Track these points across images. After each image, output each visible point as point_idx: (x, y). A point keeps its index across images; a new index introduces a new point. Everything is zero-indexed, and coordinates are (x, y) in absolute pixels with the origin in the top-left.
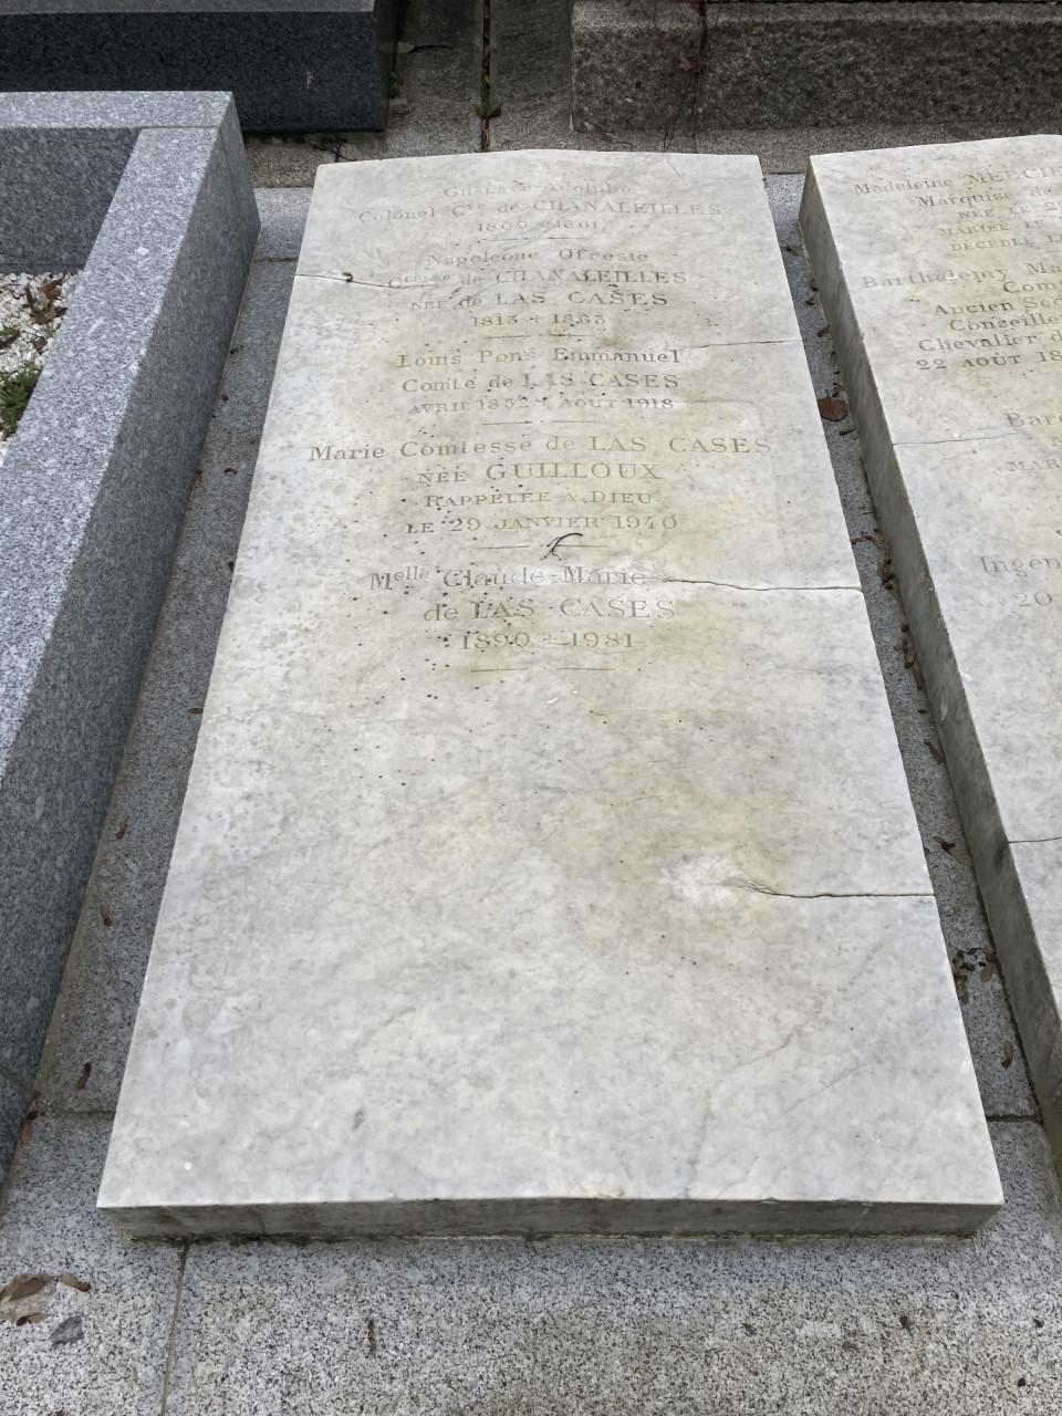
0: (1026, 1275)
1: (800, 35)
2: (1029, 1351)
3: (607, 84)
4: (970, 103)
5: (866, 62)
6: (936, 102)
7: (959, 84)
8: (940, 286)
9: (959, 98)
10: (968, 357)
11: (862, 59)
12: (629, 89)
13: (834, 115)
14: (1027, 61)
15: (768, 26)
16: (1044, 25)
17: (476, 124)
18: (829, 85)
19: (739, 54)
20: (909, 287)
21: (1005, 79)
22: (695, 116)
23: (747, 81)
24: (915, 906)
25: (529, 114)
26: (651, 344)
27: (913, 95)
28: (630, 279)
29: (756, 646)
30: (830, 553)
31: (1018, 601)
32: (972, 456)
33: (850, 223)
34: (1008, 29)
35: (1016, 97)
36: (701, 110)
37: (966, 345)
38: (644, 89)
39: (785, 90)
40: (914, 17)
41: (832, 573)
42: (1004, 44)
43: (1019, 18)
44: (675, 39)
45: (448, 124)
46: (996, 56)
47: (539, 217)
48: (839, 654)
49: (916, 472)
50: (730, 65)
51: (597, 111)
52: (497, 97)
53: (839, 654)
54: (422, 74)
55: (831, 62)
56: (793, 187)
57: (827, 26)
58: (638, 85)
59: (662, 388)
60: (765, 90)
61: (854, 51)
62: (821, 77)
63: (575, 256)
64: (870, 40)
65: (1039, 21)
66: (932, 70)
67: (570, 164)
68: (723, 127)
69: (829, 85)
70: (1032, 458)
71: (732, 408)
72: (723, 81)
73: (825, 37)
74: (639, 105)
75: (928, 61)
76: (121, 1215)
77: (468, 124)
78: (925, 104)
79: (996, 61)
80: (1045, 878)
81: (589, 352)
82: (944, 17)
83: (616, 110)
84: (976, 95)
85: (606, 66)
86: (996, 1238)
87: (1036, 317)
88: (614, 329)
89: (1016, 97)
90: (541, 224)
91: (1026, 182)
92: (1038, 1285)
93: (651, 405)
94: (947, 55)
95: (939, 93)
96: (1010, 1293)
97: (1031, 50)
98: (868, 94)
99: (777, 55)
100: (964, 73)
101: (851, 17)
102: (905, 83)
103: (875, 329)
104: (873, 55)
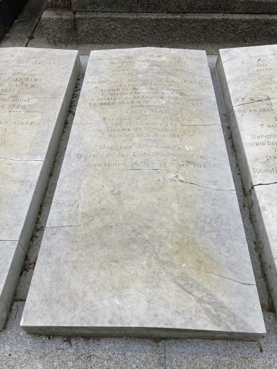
0: (12, 342)
1: (99, 21)
2: (5, 362)
3: (53, 31)
4: (147, 39)
5: (118, 28)
6: (138, 38)
7: (142, 34)
8: (105, 84)
9: (144, 37)
10: (102, 103)
11: (116, 27)
12: (59, 33)
13: (112, 41)
14: (159, 28)
15: (90, 18)
16: (161, 19)
17: (27, 40)
18: (110, 33)
19: (85, 25)
20: (97, 84)
21: (154, 33)
22: (77, 40)
23: (89, 32)
24: (11, 244)
25: (40, 38)
26: (24, 97)
27: (131, 36)
28: (28, 80)
29: (8, 175)
30: (41, 152)
31: (81, 165)
32: (90, 128)
33: (91, 68)
34: (152, 20)
35: (158, 38)
36: (78, 39)
37: (104, 99)
38: (63, 33)
39: (99, 34)
40: (127, 16)
41: (38, 157)
42: (152, 24)
43: (154, 17)
44: (67, 20)
45: (19, 40)
46: (150, 27)
47: (13, 64)
48: (28, 178)
49: (74, 131)
50: (83, 28)
51: (52, 38)
52: (35, 35)
53: (28, 178)
54: (17, 28)
55: (109, 28)
56: (214, 59)
57: (105, 18)
58: (61, 32)
59: (21, 108)
60: (94, 34)
61: (114, 25)
62: (107, 31)
63: (16, 74)
64: (117, 22)
65: (160, 18)
66: (135, 30)
67: (28, 51)
68: (86, 43)
69: (110, 33)
70: (104, 129)
71: (36, 114)
72: (82, 32)
73: (106, 21)
74: (63, 37)
75: (133, 28)
76: (25, 328)
77: (24, 41)
78: (135, 38)
79: (151, 28)
80: (49, 237)
81: (6, 99)
82: (135, 17)
83: (57, 38)
84: (148, 37)
85: (51, 27)
86: (9, 332)
87: (124, 93)
88: (16, 93)
89: (158, 38)
90: (12, 66)
91: (139, 59)
92: (14, 345)
93: (15, 112)
94: (137, 26)
95: (138, 36)
96: (6, 347)
97: (159, 25)
98: (120, 36)
99: (95, 26)
100: (143, 31)
101: (111, 16)
102: (129, 33)
103: (83, 95)
104: (119, 26)
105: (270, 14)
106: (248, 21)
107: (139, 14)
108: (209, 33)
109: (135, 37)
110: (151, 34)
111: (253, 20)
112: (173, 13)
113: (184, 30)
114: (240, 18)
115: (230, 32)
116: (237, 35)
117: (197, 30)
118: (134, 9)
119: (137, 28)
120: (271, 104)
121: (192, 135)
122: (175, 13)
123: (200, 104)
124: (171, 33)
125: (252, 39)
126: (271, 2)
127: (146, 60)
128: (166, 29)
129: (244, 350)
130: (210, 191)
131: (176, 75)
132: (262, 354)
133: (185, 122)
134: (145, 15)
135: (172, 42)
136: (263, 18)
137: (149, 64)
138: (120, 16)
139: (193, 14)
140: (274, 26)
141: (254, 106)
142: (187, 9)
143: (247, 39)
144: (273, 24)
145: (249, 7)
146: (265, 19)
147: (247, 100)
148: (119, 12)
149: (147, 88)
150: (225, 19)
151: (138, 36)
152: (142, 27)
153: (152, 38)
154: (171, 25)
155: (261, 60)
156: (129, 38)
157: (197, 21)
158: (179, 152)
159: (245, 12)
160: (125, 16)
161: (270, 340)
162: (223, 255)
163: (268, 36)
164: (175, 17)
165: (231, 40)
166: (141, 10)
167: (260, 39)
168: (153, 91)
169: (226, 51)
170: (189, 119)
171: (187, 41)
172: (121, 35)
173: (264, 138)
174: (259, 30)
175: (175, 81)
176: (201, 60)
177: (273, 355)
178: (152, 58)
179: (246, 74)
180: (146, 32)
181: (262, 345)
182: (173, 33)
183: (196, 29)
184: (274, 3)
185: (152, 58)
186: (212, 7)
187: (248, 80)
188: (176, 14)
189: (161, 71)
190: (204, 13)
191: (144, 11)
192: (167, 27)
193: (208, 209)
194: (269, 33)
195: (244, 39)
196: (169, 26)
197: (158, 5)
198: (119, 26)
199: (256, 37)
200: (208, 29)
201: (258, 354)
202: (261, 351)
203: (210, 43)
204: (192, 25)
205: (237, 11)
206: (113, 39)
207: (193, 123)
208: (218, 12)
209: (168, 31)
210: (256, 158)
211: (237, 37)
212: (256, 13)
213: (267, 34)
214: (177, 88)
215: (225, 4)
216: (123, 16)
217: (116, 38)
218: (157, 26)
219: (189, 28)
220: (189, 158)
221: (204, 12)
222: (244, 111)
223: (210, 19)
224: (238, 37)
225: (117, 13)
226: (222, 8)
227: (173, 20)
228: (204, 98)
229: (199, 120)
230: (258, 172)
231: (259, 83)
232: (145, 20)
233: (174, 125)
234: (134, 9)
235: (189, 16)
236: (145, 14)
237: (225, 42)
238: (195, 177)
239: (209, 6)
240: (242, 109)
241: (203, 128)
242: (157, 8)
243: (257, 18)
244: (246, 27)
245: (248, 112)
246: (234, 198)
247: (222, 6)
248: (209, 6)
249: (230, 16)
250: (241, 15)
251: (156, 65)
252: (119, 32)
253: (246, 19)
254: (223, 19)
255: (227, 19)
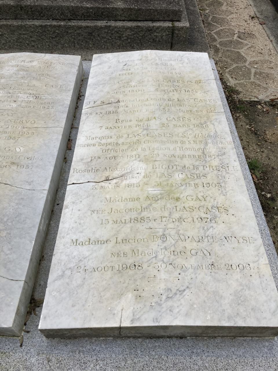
7: (31, 40)
9: (33, 44)
11: (4, 33)
13: (3, 47)
14: (46, 34)
40: (12, 23)
42: (37, 30)
65: (44, 24)
66: (23, 36)
75: (20, 34)
76: (41, 331)
78: (25, 44)
79: (38, 34)
82: (20, 23)
89: (47, 44)
94: (24, 32)
97: (45, 32)
98: (9, 42)
100: (31, 37)
102: (17, 39)
104: (6, 32)
105: (153, 21)
106: (130, 28)
107: (24, 21)
108: (95, 39)
109: (24, 43)
110: (39, 40)
111: (135, 27)
112: (58, 19)
113: (71, 36)
114: (122, 25)
115: (115, 38)
116: (123, 42)
117: (83, 36)
118: (19, 16)
119: (24, 34)
120: (118, 107)
121: (29, 137)
122: (60, 20)
123: (51, 107)
124: (59, 40)
125: (139, 46)
126: (150, 9)
127: (16, 65)
128: (53, 35)
129: (4, 345)
130: (22, 191)
131: (40, 80)
132: (21, 349)
133: (28, 125)
134: (31, 22)
135: (62, 48)
136: (144, 25)
137: (17, 69)
138: (5, 23)
139: (78, 21)
140: (157, 33)
141: (102, 109)
142: (71, 16)
143: (134, 46)
144: (155, 31)
145: (131, 14)
146: (146, 25)
147: (99, 103)
148: (6, 19)
149: (4, 92)
150: (107, 26)
151: (27, 42)
152: (28, 34)
153: (41, 44)
154: (57, 31)
155: (126, 65)
156: (19, 44)
157: (82, 28)
158: (8, 154)
159: (128, 19)
160: (10, 22)
161: (34, 335)
162: (3, 253)
163: (153, 42)
164: (59, 24)
165: (119, 46)
166: (26, 17)
167: (147, 45)
168: (9, 95)
169: (99, 57)
170: (33, 122)
171: (76, 47)
172: (10, 41)
173: (97, 139)
174: (144, 37)
175: (36, 85)
176: (72, 65)
177: (32, 350)
178: (23, 63)
179: (107, 78)
180: (34, 39)
181: (24, 340)
182: (61, 39)
183: (82, 35)
184: (153, 9)
185: (23, 63)
186: (94, 14)
187: (107, 84)
188: (61, 21)
189: (26, 76)
190: (89, 20)
191: (29, 18)
192: (53, 33)
193: (10, 209)
194: (154, 40)
195: (131, 46)
196: (54, 32)
197: (42, 12)
198: (6, 32)
199: (142, 43)
200: (94, 36)
201: (17, 349)
202: (21, 346)
203: (100, 49)
204: (78, 31)
205: (119, 18)
206: (3, 45)
207: (35, 125)
208: (102, 19)
209: (56, 37)
210: (81, 159)
211: (124, 43)
212: (139, 20)
213: (151, 40)
214: (34, 92)
215: (107, 11)
216: (8, 23)
217: (6, 44)
218: (43, 32)
219: (76, 35)
220: (15, 160)
221: (89, 19)
222: (91, 114)
223: (93, 26)
224: (125, 43)
225: (3, 20)
226: (105, 15)
227: (57, 26)
228: (58, 102)
229: (43, 122)
230: (77, 172)
231: (116, 86)
232: (30, 27)
233: (15, 127)
234: (19, 16)
235: (74, 23)
236: (31, 20)
237: (114, 48)
238: (13, 178)
239: (92, 13)
240: (90, 112)
241: (43, 131)
242: (42, 15)
243: (138, 25)
244: (130, 34)
245: (94, 114)
246: (43, 197)
247: (104, 14)
248: (92, 12)
249: (113, 24)
250: (124, 22)
251: (23, 70)
252: (7, 38)
253: (128, 26)
254: (106, 26)
255: (110, 26)
